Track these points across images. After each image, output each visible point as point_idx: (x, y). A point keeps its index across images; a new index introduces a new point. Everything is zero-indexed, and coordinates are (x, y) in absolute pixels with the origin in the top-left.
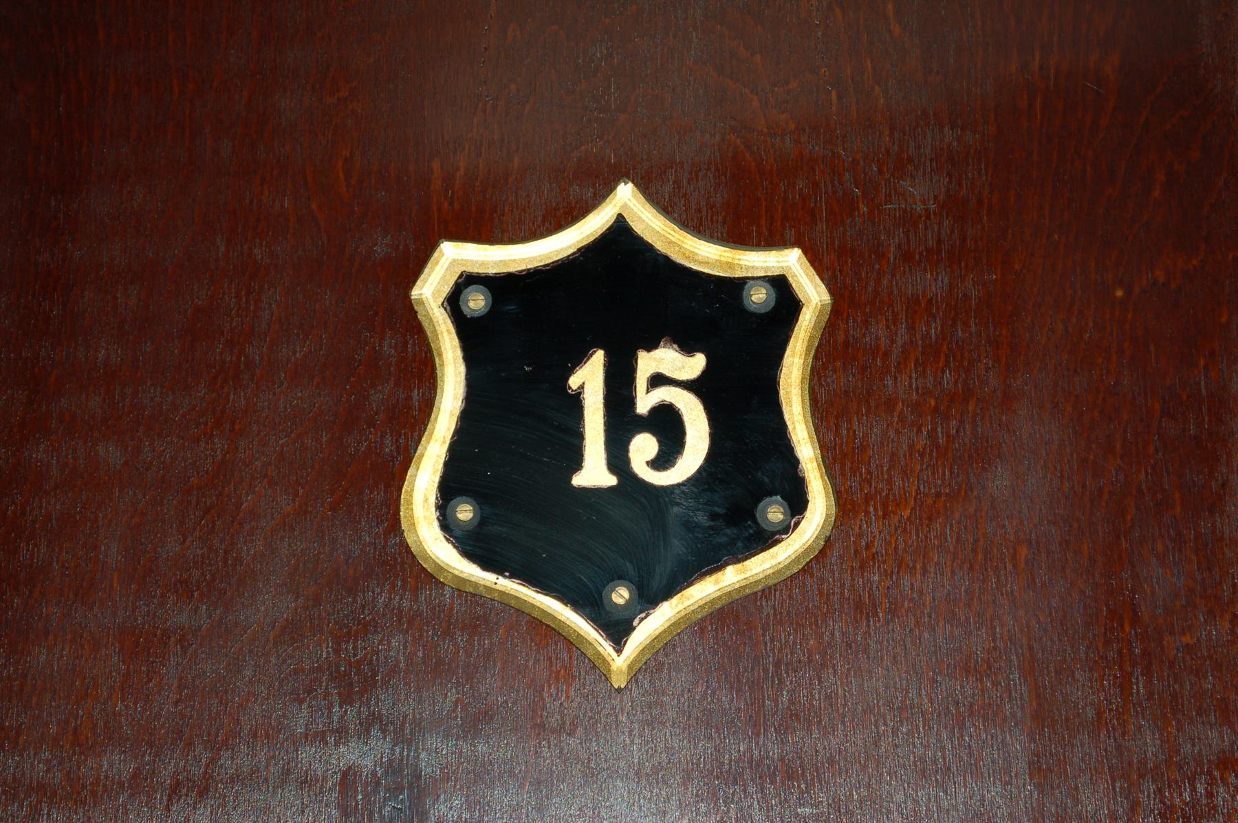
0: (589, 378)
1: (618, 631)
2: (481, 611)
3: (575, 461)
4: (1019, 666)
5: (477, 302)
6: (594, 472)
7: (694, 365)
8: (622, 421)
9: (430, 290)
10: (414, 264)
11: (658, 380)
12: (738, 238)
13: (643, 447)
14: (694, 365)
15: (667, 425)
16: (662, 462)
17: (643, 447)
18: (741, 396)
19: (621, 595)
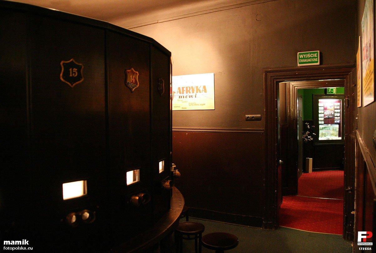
0: (71, 70)
1: (72, 85)
2: (64, 83)
3: (70, 74)
4: (137, 88)
5: (65, 64)
6: (71, 75)
7: (76, 70)
8: (73, 73)
9: (62, 63)
10: (61, 62)
11: (74, 70)
12: (76, 85)
13: (74, 74)
14: (76, 70)
15: (75, 73)
16: (75, 75)
17: (74, 74)
18: (79, 71)
19: (73, 83)
